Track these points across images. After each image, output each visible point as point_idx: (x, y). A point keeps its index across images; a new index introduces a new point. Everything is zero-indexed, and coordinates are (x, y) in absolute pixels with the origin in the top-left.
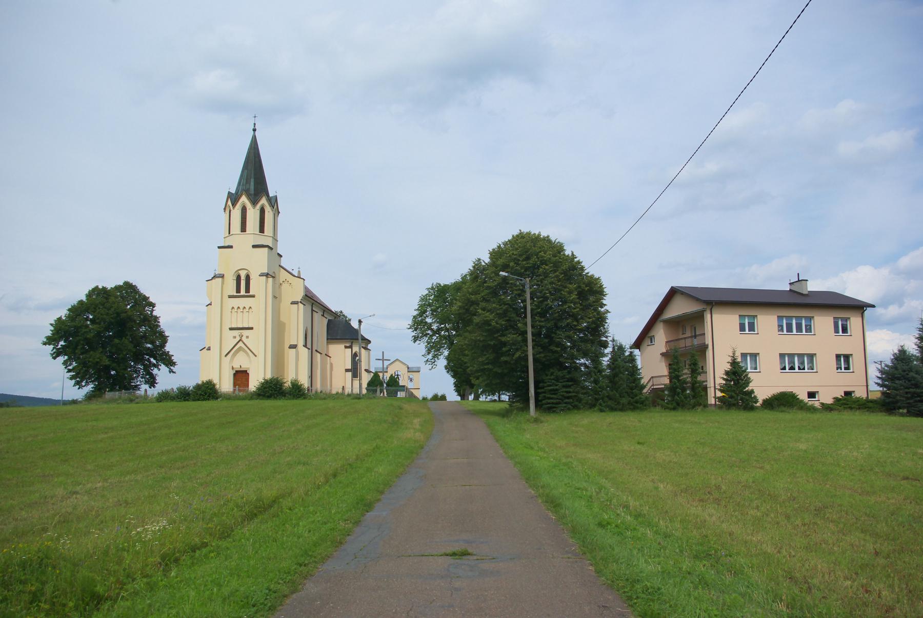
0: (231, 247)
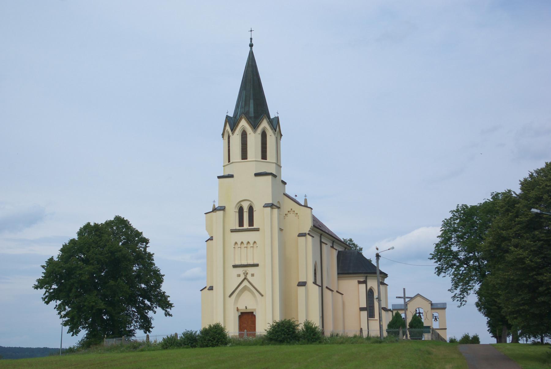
0: (231, 176)
